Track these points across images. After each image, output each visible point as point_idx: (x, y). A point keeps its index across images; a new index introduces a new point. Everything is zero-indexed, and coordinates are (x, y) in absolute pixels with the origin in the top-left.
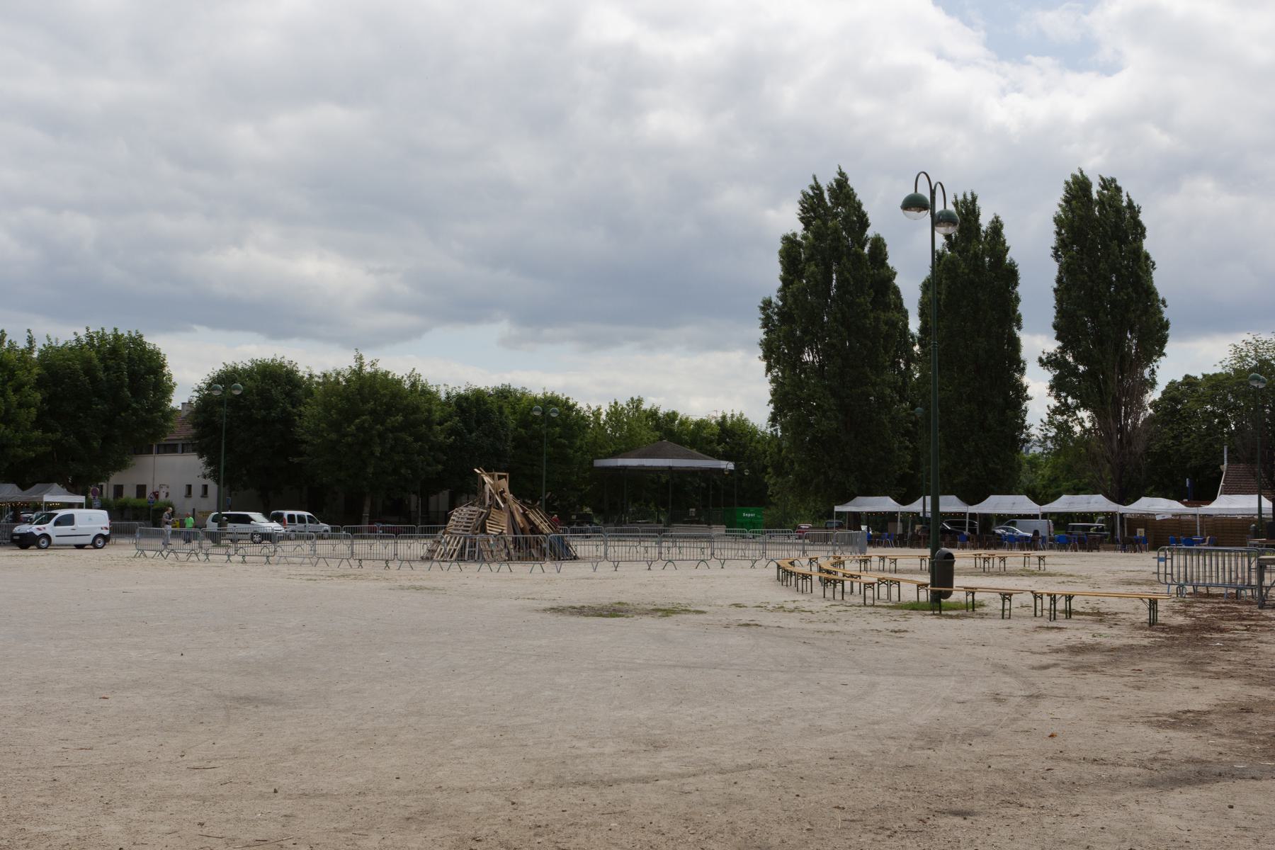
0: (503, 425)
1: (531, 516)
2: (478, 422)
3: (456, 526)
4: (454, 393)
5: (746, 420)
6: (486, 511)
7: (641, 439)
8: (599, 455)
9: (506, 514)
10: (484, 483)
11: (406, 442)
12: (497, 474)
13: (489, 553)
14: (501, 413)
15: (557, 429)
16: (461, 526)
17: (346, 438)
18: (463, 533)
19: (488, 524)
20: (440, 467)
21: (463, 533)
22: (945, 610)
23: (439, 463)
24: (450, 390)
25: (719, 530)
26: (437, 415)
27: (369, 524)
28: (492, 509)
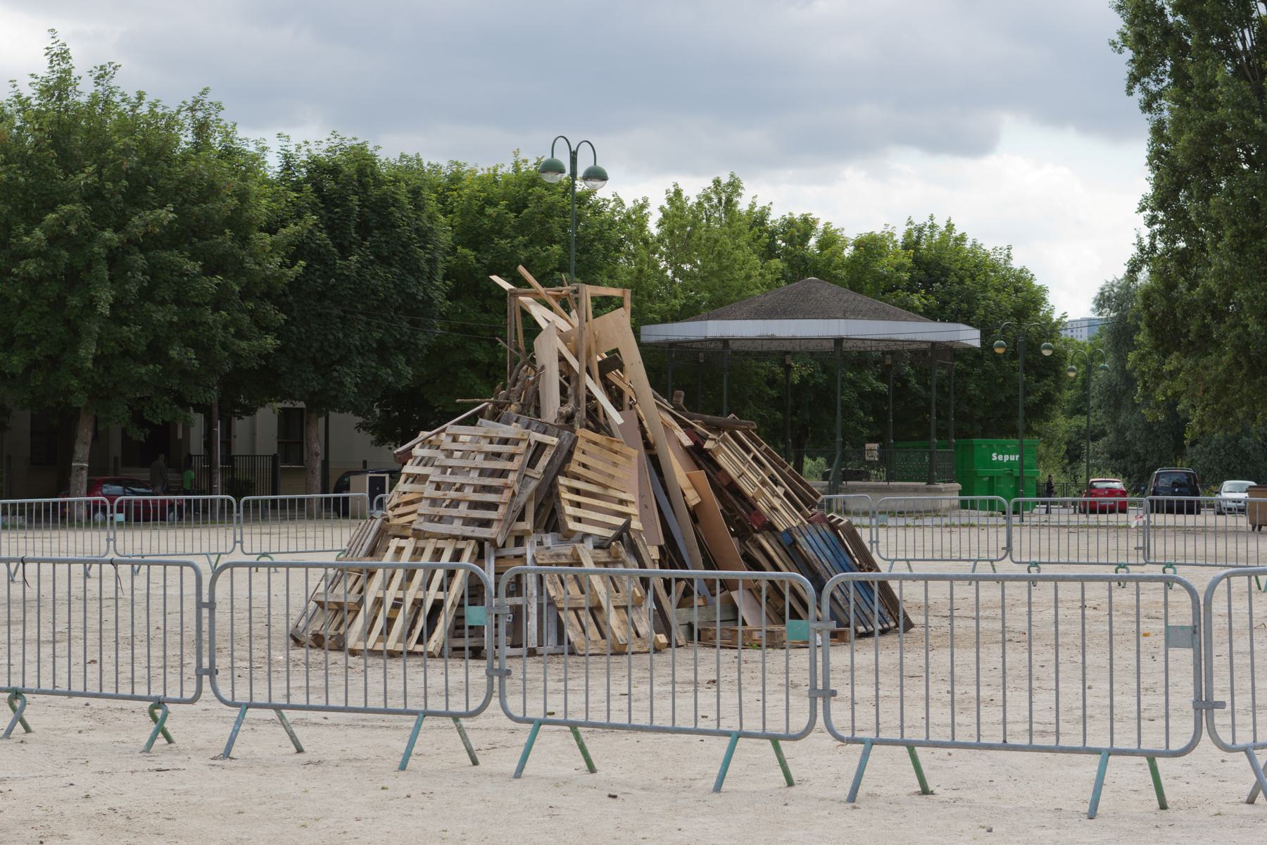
0: (424, 235)
1: (729, 460)
2: (364, 229)
3: (434, 502)
4: (303, 157)
5: (962, 238)
6: (552, 440)
7: (748, 277)
8: (650, 315)
9: (634, 453)
10: (532, 329)
11: (182, 275)
12: (589, 291)
13: (586, 618)
14: (419, 207)
15: (556, 247)
16: (455, 503)
17: (23, 263)
18: (468, 531)
19: (566, 495)
20: (270, 342)
21: (468, 531)
22: (77, 461)
23: (267, 330)
24: (292, 150)
25: (949, 494)
26: (262, 209)
27: (88, 495)
28: (583, 433)
